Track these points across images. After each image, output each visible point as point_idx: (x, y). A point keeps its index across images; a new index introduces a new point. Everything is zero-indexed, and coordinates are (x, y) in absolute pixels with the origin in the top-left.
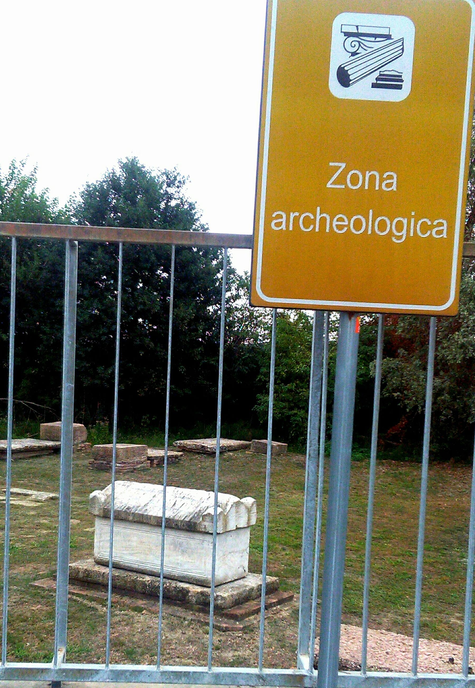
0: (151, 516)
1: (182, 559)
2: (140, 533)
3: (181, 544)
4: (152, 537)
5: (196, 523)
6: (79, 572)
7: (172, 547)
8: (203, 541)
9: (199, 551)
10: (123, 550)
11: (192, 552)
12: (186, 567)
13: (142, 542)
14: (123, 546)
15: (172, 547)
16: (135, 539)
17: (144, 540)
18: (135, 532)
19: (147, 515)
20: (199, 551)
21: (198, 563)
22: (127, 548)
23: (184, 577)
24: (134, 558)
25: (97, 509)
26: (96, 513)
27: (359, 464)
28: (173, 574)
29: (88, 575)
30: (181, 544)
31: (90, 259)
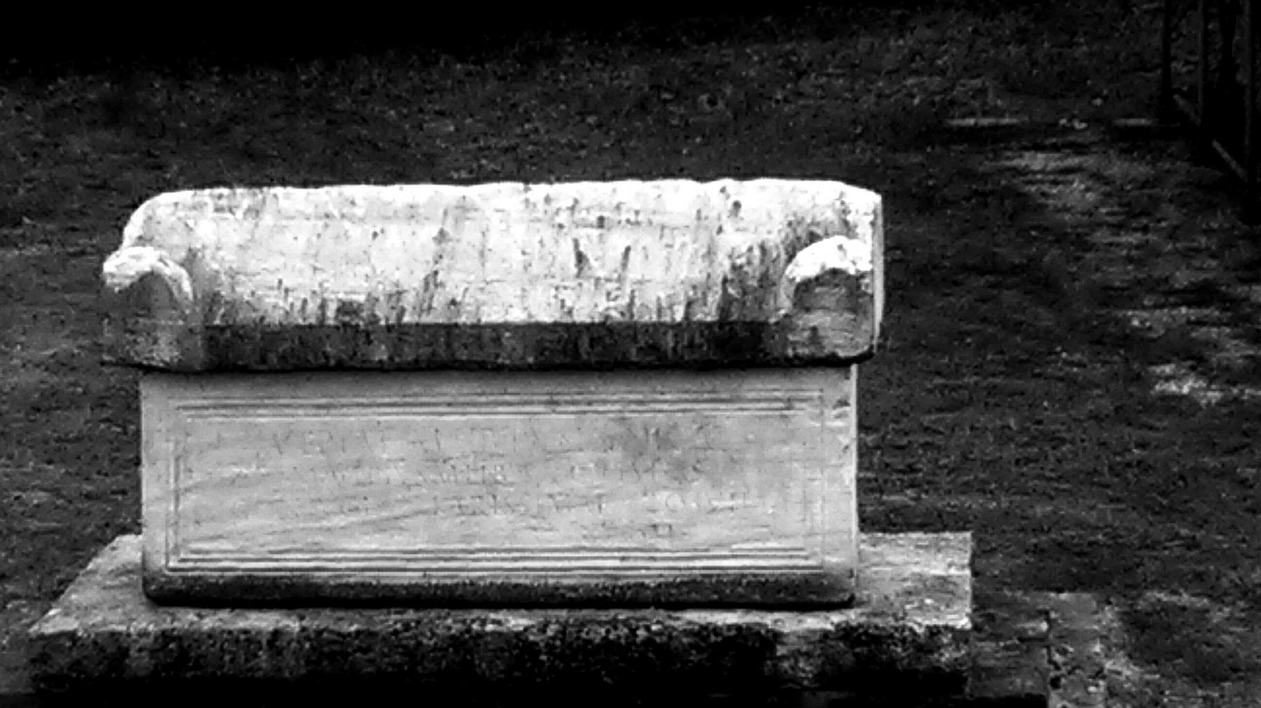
0: (497, 328)
1: (676, 501)
2: (419, 419)
3: (664, 440)
4: (571, 424)
5: (765, 324)
6: (124, 652)
7: (615, 456)
8: (789, 403)
9: (773, 451)
10: (327, 514)
11: (734, 463)
12: (702, 534)
13: (436, 460)
14: (325, 493)
15: (615, 456)
16: (393, 448)
17: (449, 446)
18: (391, 418)
19: (473, 326)
20: (773, 451)
21: (767, 508)
22: (347, 501)
23: (693, 584)
24: (396, 542)
25: (164, 338)
26: (165, 353)
27: (1074, 664)
28: (632, 577)
29: (184, 653)
30: (664, 440)
31: (938, 67)
